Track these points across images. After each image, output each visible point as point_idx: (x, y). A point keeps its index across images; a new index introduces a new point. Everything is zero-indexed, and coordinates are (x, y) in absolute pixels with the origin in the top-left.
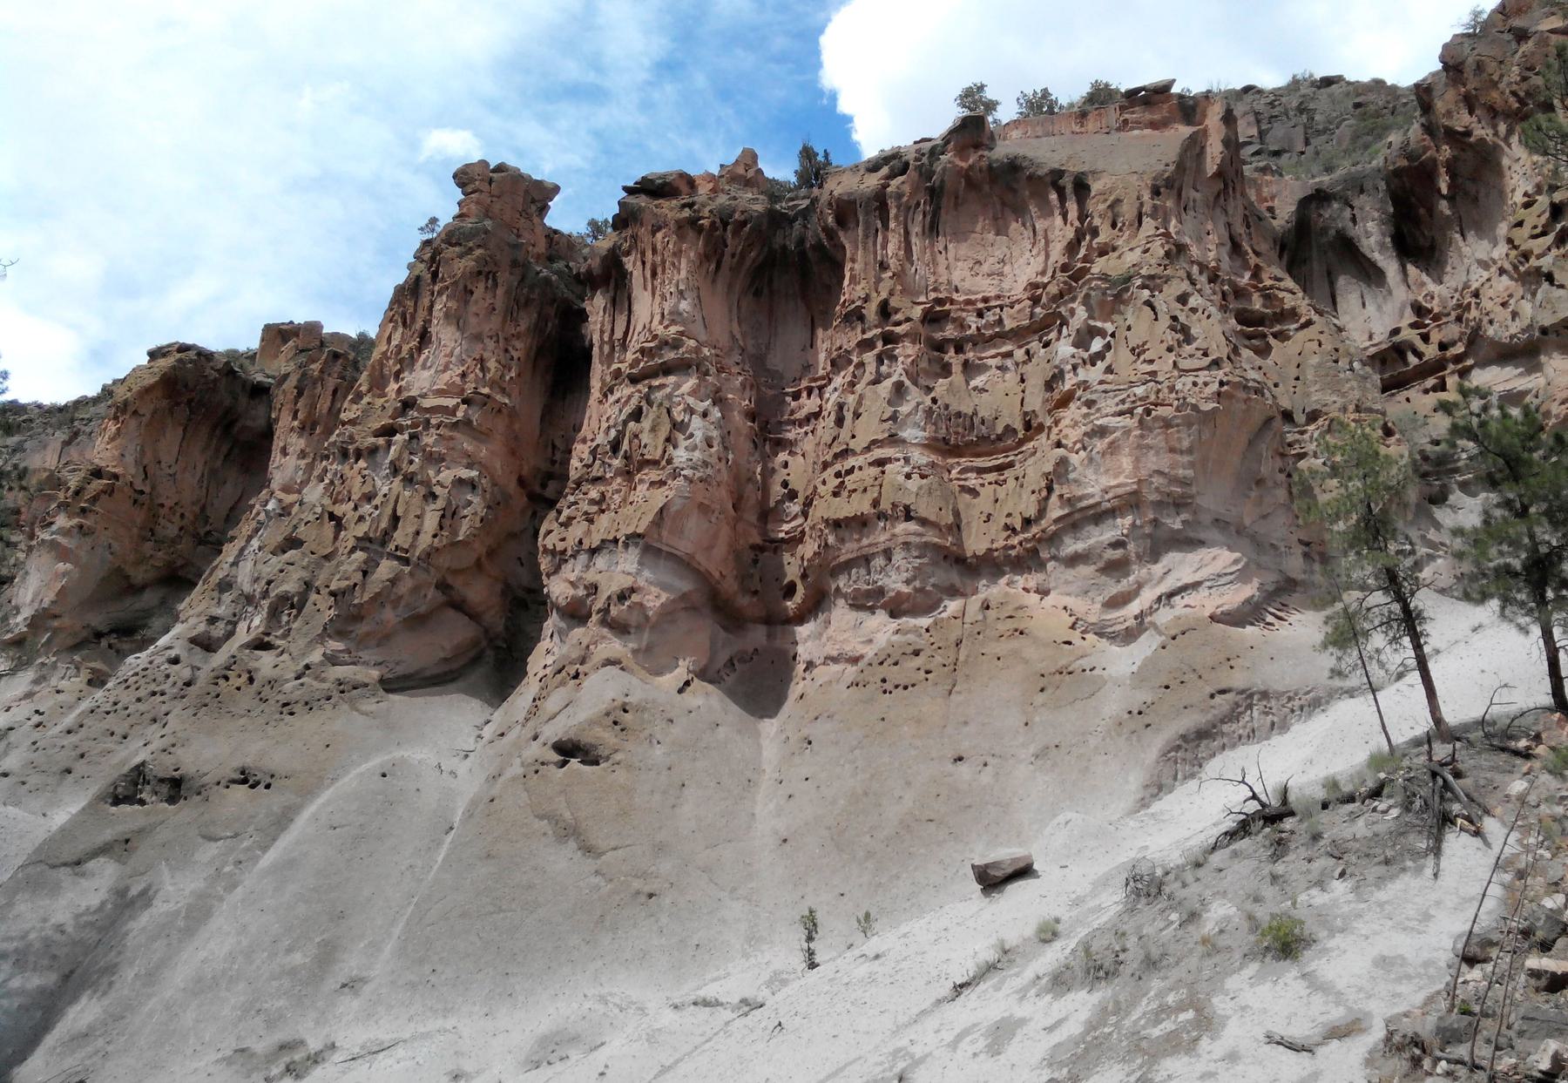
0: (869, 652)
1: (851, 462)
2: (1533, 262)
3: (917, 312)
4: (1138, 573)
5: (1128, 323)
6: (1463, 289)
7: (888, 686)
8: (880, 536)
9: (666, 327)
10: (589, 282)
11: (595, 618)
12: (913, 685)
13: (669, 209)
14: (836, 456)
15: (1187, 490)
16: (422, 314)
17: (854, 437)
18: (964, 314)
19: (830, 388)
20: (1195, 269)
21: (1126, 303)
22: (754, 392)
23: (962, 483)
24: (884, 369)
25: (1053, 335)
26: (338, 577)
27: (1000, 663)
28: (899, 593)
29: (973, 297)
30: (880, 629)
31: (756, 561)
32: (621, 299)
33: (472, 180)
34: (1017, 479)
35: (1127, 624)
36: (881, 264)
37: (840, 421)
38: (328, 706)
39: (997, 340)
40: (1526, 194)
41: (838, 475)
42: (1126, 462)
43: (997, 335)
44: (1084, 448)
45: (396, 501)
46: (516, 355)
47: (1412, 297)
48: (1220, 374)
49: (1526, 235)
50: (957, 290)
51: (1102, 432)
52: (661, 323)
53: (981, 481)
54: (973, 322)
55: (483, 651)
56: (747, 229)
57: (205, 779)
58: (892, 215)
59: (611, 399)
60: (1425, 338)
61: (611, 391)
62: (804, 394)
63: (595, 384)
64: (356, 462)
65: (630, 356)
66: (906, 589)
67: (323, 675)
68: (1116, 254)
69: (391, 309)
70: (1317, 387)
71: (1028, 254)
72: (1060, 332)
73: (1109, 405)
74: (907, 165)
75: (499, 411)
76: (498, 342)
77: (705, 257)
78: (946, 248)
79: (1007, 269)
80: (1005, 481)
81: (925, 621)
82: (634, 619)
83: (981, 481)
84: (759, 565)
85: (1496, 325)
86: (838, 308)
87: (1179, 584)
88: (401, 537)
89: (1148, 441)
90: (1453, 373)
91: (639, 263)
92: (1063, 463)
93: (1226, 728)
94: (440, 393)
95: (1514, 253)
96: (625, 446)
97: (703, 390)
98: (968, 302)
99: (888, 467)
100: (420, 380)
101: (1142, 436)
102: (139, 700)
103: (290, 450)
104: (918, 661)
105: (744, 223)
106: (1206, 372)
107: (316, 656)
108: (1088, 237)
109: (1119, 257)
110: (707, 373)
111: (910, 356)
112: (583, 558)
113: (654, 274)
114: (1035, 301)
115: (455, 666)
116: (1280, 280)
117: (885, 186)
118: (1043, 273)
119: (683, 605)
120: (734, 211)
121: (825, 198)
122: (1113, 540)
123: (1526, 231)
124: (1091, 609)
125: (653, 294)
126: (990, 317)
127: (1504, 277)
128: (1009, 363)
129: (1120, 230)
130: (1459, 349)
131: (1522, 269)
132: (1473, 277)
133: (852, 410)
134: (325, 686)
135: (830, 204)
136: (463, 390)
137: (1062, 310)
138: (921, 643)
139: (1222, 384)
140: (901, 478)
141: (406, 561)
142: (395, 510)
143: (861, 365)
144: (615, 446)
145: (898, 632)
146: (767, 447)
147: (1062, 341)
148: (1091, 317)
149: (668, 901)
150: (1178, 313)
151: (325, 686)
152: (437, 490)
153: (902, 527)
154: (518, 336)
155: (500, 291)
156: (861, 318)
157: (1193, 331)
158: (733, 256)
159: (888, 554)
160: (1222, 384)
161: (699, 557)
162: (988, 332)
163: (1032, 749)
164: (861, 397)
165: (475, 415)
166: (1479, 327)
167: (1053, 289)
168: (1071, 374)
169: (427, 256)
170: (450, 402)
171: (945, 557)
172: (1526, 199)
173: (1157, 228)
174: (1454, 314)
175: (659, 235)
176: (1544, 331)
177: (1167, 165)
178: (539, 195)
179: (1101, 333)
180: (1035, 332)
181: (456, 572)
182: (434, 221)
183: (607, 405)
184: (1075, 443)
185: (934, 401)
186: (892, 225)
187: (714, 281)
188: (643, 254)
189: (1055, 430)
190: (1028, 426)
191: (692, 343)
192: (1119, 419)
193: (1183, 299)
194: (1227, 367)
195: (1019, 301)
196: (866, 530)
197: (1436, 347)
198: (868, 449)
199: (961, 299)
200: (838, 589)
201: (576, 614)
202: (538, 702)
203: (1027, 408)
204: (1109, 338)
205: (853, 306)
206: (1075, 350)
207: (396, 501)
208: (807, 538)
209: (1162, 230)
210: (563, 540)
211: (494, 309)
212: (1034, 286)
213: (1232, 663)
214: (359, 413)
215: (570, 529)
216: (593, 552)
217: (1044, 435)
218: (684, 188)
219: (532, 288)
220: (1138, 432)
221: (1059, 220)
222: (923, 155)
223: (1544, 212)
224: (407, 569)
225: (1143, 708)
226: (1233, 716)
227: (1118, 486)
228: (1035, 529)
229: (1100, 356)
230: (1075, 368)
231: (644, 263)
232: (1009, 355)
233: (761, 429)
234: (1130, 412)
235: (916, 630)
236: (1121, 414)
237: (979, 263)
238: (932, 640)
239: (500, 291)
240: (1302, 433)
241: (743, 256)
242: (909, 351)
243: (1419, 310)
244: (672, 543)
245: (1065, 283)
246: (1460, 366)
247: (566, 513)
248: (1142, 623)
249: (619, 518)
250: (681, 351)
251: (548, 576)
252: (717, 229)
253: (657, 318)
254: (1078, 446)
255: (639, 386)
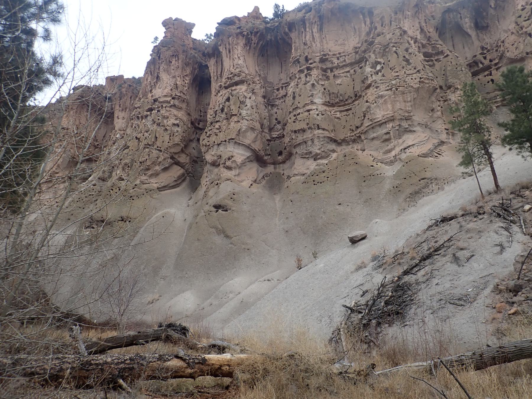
0: (308, 172)
1: (299, 111)
2: (524, 30)
3: (317, 59)
4: (394, 142)
5: (389, 59)
6: (498, 40)
7: (316, 183)
8: (308, 135)
9: (235, 70)
10: (209, 56)
11: (221, 166)
12: (323, 182)
13: (233, 29)
14: (294, 109)
15: (409, 114)
16: (157, 71)
17: (299, 103)
18: (333, 59)
19: (290, 87)
20: (410, 39)
21: (388, 52)
22: (264, 89)
23: (335, 116)
24: (308, 79)
25: (363, 64)
26: (141, 157)
27: (350, 173)
28: (317, 153)
29: (335, 53)
30: (312, 165)
31: (269, 145)
32: (220, 61)
33: (168, 24)
34: (353, 114)
35: (391, 159)
36: (304, 43)
37: (294, 98)
38: (143, 197)
39: (344, 67)
40: (522, 6)
41: (295, 116)
42: (390, 106)
43: (344, 66)
44: (376, 102)
45: (156, 132)
46: (187, 82)
47: (480, 44)
48: (420, 75)
49: (522, 20)
50: (330, 51)
51: (382, 97)
52: (233, 68)
53: (341, 115)
54: (336, 61)
55: (186, 177)
56: (259, 34)
57: (111, 220)
58: (307, 27)
59: (219, 95)
60: (485, 58)
61: (219, 92)
62: (281, 89)
63: (213, 90)
64: (142, 120)
65: (224, 80)
66: (318, 152)
67: (141, 187)
68: (383, 35)
69: (146, 70)
70: (451, 77)
71: (353, 37)
72: (366, 63)
73: (383, 87)
74: (311, 8)
75: (184, 101)
76: (181, 78)
77: (246, 45)
78: (325, 36)
79: (346, 42)
80: (349, 114)
81: (325, 161)
82: (233, 165)
83: (341, 115)
84: (270, 146)
85: (510, 52)
86: (291, 59)
87: (408, 145)
88: (158, 143)
89: (397, 99)
90: (494, 69)
91: (224, 49)
92: (369, 107)
93: (424, 190)
94: (165, 96)
95: (517, 27)
96: (226, 110)
97: (249, 90)
98: (334, 55)
99: (311, 112)
100: (158, 92)
101: (395, 97)
102: (86, 197)
103: (120, 117)
104: (324, 174)
105: (257, 32)
106: (415, 75)
107: (138, 182)
108: (373, 30)
109: (384, 36)
110: (249, 84)
111: (316, 74)
112: (216, 147)
113: (230, 52)
114: (356, 53)
115: (178, 182)
116: (437, 41)
117: (304, 17)
118: (358, 43)
119: (249, 160)
120: (254, 29)
121: (284, 22)
122: (386, 132)
123: (522, 18)
124: (379, 155)
125: (230, 59)
126: (341, 59)
127: (513, 35)
128: (348, 74)
129: (384, 27)
130: (497, 61)
131: (520, 32)
132: (502, 36)
133: (298, 94)
134: (142, 191)
135: (286, 24)
136: (172, 95)
137: (366, 56)
138: (325, 169)
139: (421, 78)
140: (315, 116)
141: (161, 151)
142: (156, 135)
143: (300, 78)
144: (222, 110)
145: (317, 165)
146: (270, 107)
147: (367, 67)
148: (376, 58)
149: (253, 251)
150: (405, 55)
151: (142, 191)
152: (168, 128)
153: (317, 132)
154: (187, 75)
155: (180, 61)
156: (299, 62)
157: (410, 61)
158: (255, 44)
159: (312, 140)
160: (421, 78)
161: (252, 145)
162: (341, 65)
163: (362, 200)
164: (301, 89)
165: (176, 102)
166: (504, 52)
167: (363, 49)
168: (370, 78)
169: (156, 51)
170: (169, 99)
171: (331, 141)
172: (522, 8)
173: (397, 26)
174: (495, 49)
175: (230, 39)
176: (527, 54)
177: (399, 3)
178: (189, 28)
179: (379, 63)
180: (357, 63)
181: (176, 153)
182: (156, 38)
183: (218, 97)
184: (372, 101)
185: (325, 89)
186: (307, 30)
187: (249, 53)
188: (225, 45)
189: (366, 97)
190: (356, 96)
191: (244, 74)
192: (387, 92)
193: (407, 50)
194: (422, 72)
195: (351, 54)
196: (305, 133)
197: (488, 61)
198: (304, 106)
199: (331, 54)
200: (296, 152)
201: (215, 164)
202: (206, 193)
203: (356, 90)
204: (382, 65)
205: (296, 59)
206: (371, 70)
207: (156, 132)
208: (285, 137)
209: (398, 26)
210: (208, 142)
211: (179, 67)
212: (356, 48)
213: (425, 170)
214: (140, 104)
215: (210, 138)
216: (219, 145)
217: (361, 99)
218: (237, 22)
219: (190, 59)
220: (393, 96)
221: (363, 25)
222: (316, 5)
223: (528, 12)
224: (161, 153)
225: (398, 186)
226: (426, 186)
227: (387, 114)
228: (359, 130)
229: (380, 71)
230: (372, 75)
231: (226, 48)
232: (349, 72)
233: (267, 101)
234: (391, 89)
235: (323, 164)
236: (387, 90)
237: (337, 41)
238: (328, 167)
239: (180, 61)
240: (445, 93)
241: (258, 43)
242: (316, 73)
243: (483, 48)
244: (243, 141)
245: (366, 46)
246: (497, 67)
247: (208, 133)
248: (395, 158)
249: (226, 134)
250: (241, 77)
251: (204, 153)
252: (249, 35)
253: (232, 67)
254: (374, 102)
255: (228, 90)
